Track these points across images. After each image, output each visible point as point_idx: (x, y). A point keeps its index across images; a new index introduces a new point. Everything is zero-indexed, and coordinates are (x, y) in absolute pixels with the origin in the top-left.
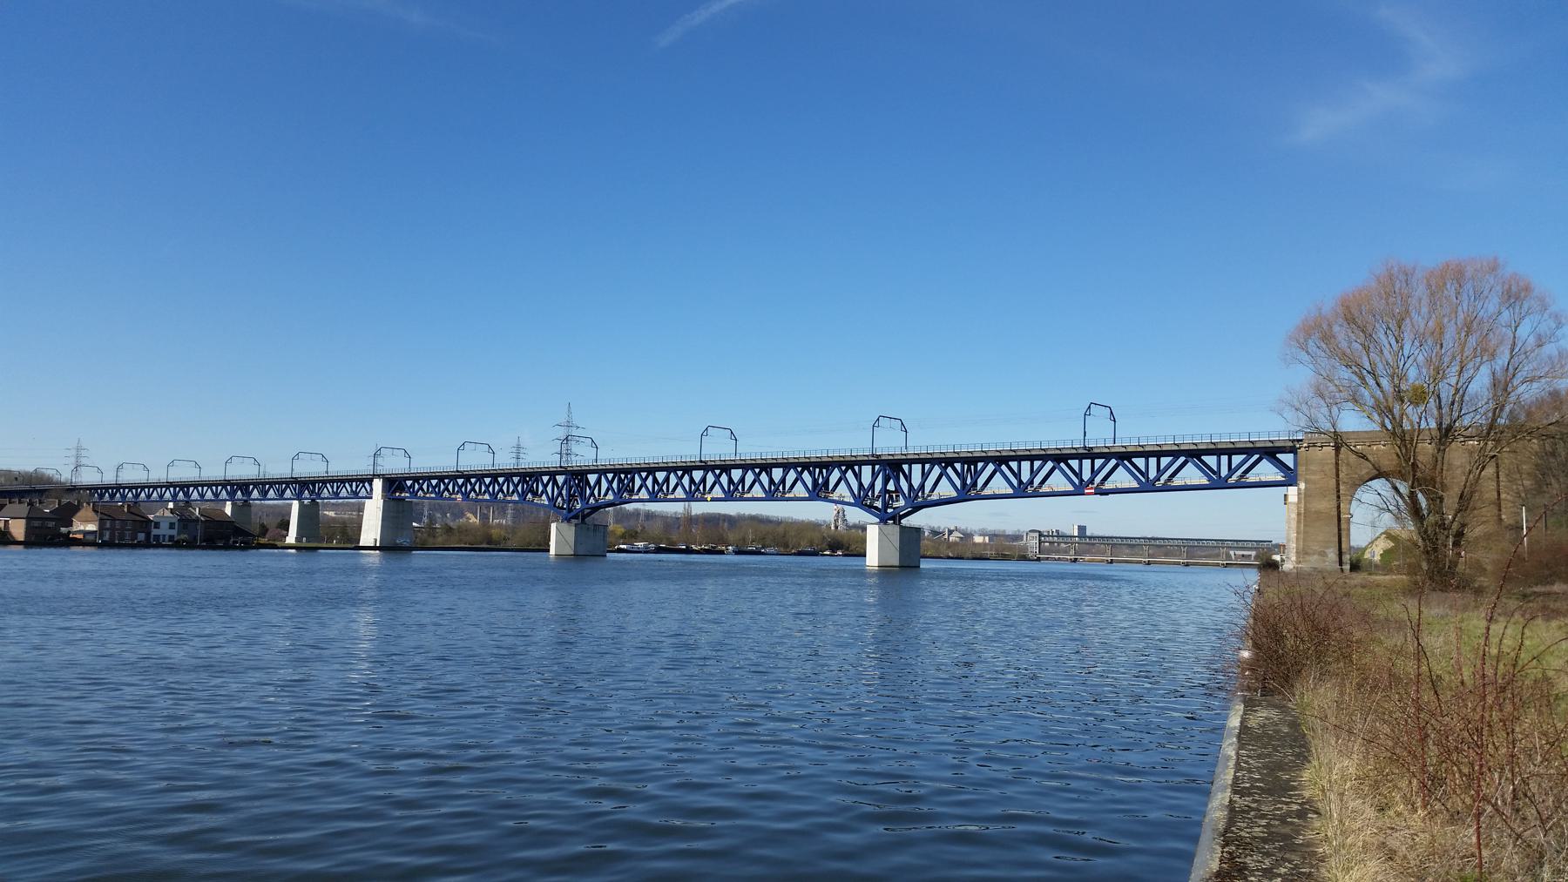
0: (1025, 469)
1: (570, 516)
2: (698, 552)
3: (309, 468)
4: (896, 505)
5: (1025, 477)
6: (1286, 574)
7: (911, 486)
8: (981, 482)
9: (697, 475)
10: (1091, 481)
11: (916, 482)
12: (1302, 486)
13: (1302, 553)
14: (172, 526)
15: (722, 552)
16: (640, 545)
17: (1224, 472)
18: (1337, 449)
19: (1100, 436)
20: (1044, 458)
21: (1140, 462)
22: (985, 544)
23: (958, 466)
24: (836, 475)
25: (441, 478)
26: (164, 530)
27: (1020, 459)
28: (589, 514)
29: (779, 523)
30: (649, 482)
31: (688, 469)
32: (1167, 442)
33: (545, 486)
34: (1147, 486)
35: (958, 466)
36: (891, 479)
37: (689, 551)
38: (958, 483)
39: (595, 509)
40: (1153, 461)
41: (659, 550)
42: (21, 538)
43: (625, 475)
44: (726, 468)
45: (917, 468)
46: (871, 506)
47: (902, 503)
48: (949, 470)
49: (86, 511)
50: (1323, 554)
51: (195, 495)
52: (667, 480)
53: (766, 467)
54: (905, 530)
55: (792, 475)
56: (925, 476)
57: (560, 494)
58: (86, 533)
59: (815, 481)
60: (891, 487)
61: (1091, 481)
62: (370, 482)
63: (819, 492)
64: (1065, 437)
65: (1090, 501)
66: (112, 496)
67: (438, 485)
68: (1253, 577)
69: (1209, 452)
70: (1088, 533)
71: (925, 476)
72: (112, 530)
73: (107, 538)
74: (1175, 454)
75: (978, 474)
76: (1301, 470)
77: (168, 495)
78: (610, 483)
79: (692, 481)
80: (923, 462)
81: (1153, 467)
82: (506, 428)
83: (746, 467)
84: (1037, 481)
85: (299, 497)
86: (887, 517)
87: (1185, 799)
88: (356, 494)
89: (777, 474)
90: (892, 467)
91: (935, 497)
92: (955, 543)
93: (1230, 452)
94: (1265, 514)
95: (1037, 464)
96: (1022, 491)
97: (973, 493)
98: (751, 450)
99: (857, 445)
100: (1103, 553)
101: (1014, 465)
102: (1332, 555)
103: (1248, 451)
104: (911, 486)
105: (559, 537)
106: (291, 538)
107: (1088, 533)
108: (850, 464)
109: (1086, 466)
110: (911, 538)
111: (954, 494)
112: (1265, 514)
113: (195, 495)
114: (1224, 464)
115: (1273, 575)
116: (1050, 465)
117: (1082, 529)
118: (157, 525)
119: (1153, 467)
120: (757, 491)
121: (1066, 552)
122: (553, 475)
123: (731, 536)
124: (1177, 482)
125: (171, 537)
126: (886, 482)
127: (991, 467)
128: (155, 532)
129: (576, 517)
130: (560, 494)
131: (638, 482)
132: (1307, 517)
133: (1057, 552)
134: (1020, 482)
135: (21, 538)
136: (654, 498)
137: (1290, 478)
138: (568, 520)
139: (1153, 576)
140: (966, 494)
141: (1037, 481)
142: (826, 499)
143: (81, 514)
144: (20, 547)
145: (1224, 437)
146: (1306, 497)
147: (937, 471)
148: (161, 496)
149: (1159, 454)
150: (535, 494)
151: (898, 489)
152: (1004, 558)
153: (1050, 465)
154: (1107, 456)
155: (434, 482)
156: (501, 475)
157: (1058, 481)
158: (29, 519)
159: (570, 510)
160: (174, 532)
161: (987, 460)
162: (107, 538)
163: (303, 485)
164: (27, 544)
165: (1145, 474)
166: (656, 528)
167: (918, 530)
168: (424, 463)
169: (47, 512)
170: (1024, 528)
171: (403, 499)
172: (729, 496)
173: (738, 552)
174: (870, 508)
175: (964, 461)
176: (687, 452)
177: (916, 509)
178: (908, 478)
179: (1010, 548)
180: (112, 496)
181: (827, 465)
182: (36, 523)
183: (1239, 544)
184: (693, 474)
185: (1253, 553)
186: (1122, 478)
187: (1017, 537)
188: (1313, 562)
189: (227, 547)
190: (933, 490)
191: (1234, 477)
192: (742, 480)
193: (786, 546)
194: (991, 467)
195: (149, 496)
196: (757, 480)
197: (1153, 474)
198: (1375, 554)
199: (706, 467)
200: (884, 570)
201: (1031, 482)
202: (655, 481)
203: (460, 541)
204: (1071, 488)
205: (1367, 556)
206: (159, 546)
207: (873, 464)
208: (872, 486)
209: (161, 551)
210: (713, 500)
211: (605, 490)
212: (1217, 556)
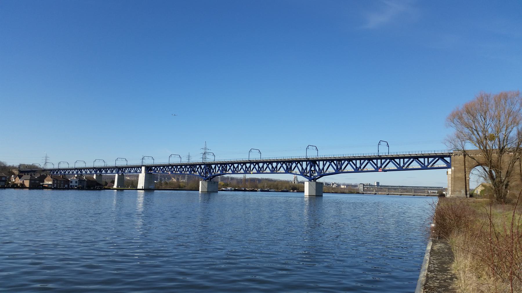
0: (359, 163)
1: (206, 179)
2: (248, 191)
4: (314, 175)
5: (358, 165)
6: (448, 198)
7: (319, 169)
9: (248, 165)
10: (381, 167)
12: (453, 168)
13: (453, 191)
14: (76, 182)
15: (256, 191)
16: (229, 188)
18: (465, 156)
19: (383, 152)
20: (365, 159)
21: (397, 160)
24: (294, 165)
25: (164, 166)
26: (74, 184)
27: (356, 159)
29: (275, 181)
30: (232, 168)
31: (245, 163)
32: (407, 154)
33: (198, 169)
34: (400, 169)
35: (335, 162)
36: (313, 166)
37: (245, 190)
38: (335, 167)
39: (214, 176)
40: (402, 160)
41: (235, 190)
42: (28, 186)
43: (224, 165)
44: (257, 163)
45: (321, 163)
46: (306, 175)
47: (316, 174)
48: (332, 163)
49: (49, 177)
50: (460, 191)
51: (84, 172)
52: (238, 167)
53: (271, 162)
54: (317, 183)
56: (324, 165)
57: (203, 171)
58: (49, 185)
59: (287, 167)
60: (313, 169)
61: (381, 167)
62: (141, 168)
63: (289, 171)
64: (372, 152)
66: (57, 173)
67: (163, 169)
68: (436, 200)
70: (380, 185)
71: (324, 165)
72: (57, 183)
73: (55, 186)
74: (409, 158)
75: (342, 164)
76: (452, 163)
77: (75, 172)
79: (246, 167)
80: (323, 160)
81: (402, 162)
83: (264, 162)
84: (362, 167)
86: (312, 179)
89: (274, 165)
90: (313, 162)
91: (327, 172)
92: (334, 188)
93: (428, 157)
94: (440, 178)
95: (362, 161)
96: (357, 170)
97: (340, 171)
98: (266, 156)
99: (301, 155)
100: (385, 191)
101: (354, 161)
102: (463, 192)
103: (434, 157)
104: (319, 169)
105: (202, 185)
107: (380, 185)
108: (299, 161)
109: (379, 162)
110: (320, 186)
111: (334, 171)
112: (440, 178)
114: (427, 161)
115: (443, 199)
116: (388, 160)
117: (378, 183)
118: (71, 182)
119: (402, 162)
121: (372, 191)
122: (200, 165)
123: (259, 185)
124: (410, 167)
126: (311, 167)
127: (346, 162)
128: (71, 184)
129: (208, 179)
130: (203, 171)
131: (228, 167)
132: (454, 179)
133: (370, 191)
134: (357, 167)
136: (233, 173)
137: (449, 166)
138: (205, 180)
140: (338, 171)
141: (362, 167)
142: (291, 173)
146: (454, 172)
147: (328, 163)
148: (73, 173)
149: (404, 158)
150: (194, 171)
151: (315, 170)
152: (351, 193)
153: (366, 161)
154: (386, 159)
159: (206, 177)
160: (77, 184)
161: (345, 160)
163: (119, 169)
164: (30, 188)
165: (399, 165)
166: (234, 183)
172: (258, 172)
174: (306, 176)
175: (337, 160)
176: (244, 157)
177: (321, 176)
178: (318, 166)
179: (353, 190)
180: (57, 173)
181: (291, 162)
182: (33, 182)
184: (246, 165)
185: (436, 191)
186: (391, 166)
187: (356, 186)
188: (457, 194)
190: (327, 170)
192: (263, 167)
193: (278, 189)
194: (346, 162)
195: (69, 172)
197: (402, 164)
198: (478, 191)
199: (251, 162)
202: (234, 167)
204: (374, 169)
207: (306, 161)
208: (306, 169)
211: (217, 170)
212: (424, 192)
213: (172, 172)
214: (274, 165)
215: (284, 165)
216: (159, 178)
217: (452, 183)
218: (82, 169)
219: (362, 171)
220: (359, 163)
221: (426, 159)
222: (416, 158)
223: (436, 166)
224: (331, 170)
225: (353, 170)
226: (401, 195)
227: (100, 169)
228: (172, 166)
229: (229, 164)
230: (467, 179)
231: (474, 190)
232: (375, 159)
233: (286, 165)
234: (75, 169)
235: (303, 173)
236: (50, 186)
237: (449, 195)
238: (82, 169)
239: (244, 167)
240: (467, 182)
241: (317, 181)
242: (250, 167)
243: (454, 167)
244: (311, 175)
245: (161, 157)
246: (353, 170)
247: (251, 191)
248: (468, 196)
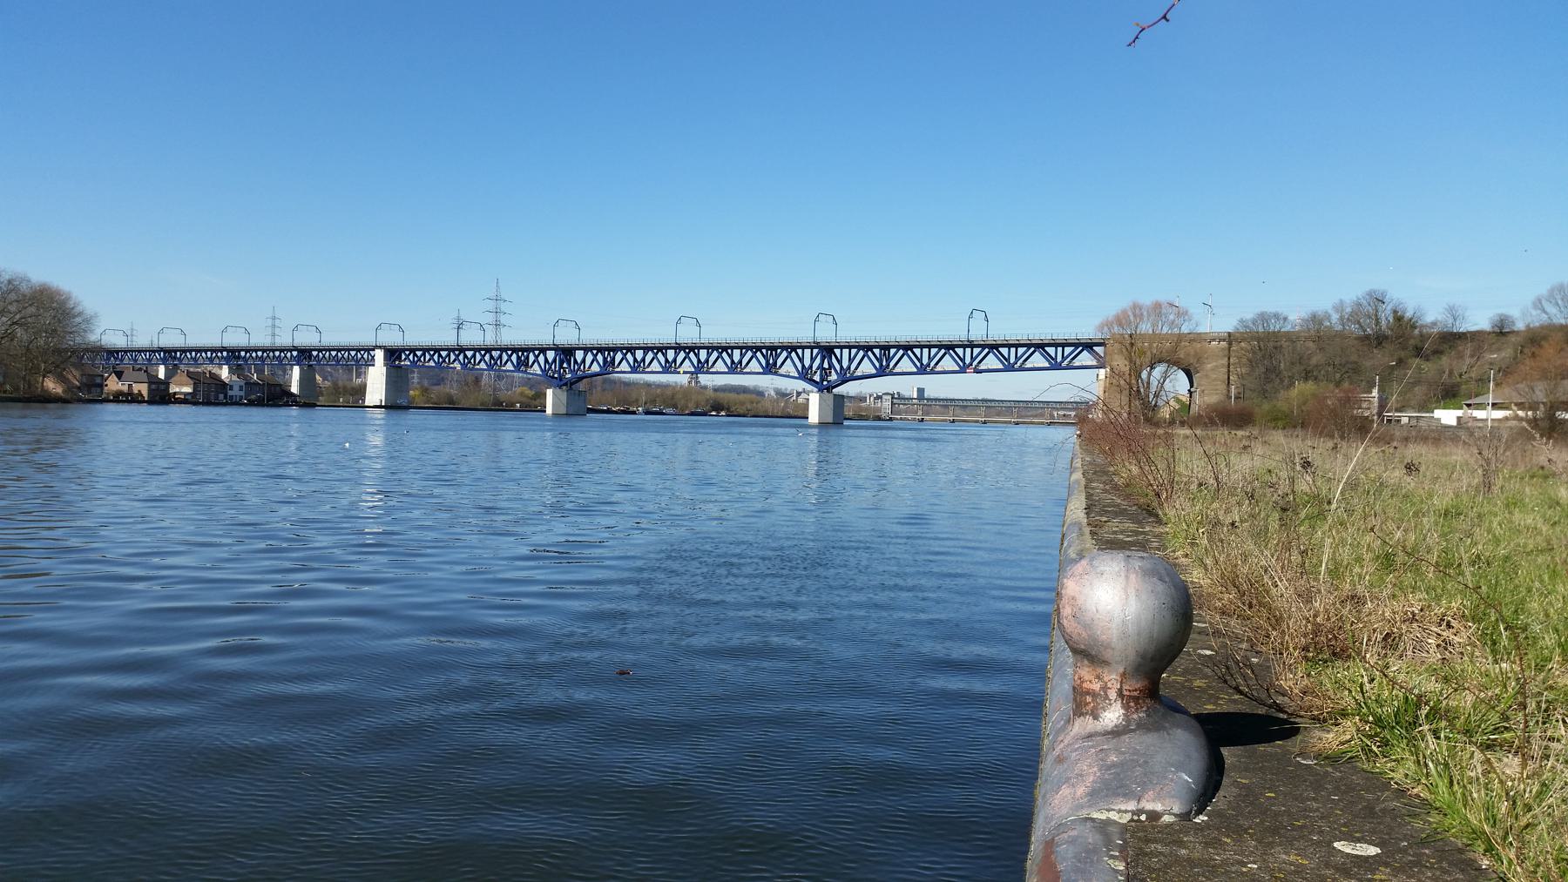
0: (926, 354)
1: (560, 383)
8: (779, 362)
9: (495, 354)
15: (634, 413)
18: (1230, 344)
19: (977, 334)
21: (1004, 351)
32: (1023, 338)
34: (1009, 368)
35: (877, 351)
36: (826, 361)
39: (581, 378)
45: (737, 353)
55: (650, 355)
56: (742, 356)
58: (186, 394)
59: (605, 359)
60: (826, 365)
63: (770, 369)
65: (970, 377)
71: (742, 356)
75: (778, 356)
80: (741, 348)
81: (1012, 354)
82: (1302, 281)
83: (710, 348)
86: (824, 388)
87: (1039, 656)
89: (639, 354)
90: (827, 350)
99: (805, 336)
124: (1028, 365)
127: (785, 354)
128: (230, 393)
131: (532, 358)
136: (634, 370)
139: (990, 434)
140: (882, 372)
141: (744, 362)
142: (776, 373)
145: (1060, 334)
147: (749, 354)
151: (831, 365)
154: (983, 347)
158: (150, 383)
161: (784, 348)
168: (412, 339)
173: (648, 413)
174: (811, 381)
176: (665, 336)
181: (615, 349)
186: (992, 361)
199: (678, 348)
200: (822, 425)
207: (812, 348)
212: (1042, 415)
214: (639, 354)
215: (629, 356)
216: (434, 382)
219: (933, 372)
222: (1040, 346)
223: (1077, 363)
224: (867, 367)
232: (1003, 346)
235: (805, 375)
239: (487, 357)
244: (822, 379)
245: (427, 328)
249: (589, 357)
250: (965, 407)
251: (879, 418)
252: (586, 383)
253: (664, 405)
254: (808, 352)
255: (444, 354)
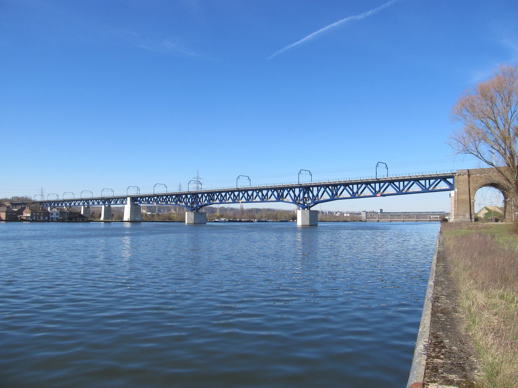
0: (354, 188)
1: (192, 209)
2: (244, 222)
3: (108, 194)
4: (308, 202)
5: (355, 190)
6: (451, 223)
7: (313, 195)
10: (379, 191)
11: (297, 194)
12: (456, 190)
13: (456, 215)
14: (57, 214)
15: (253, 222)
16: (223, 219)
17: (427, 186)
18: (469, 176)
19: (382, 175)
20: (362, 183)
21: (397, 184)
22: (347, 216)
23: (330, 187)
24: (286, 192)
25: (149, 197)
26: (54, 216)
27: (353, 184)
28: (199, 209)
29: (274, 210)
30: (232, 196)
31: (233, 192)
32: (406, 175)
33: (184, 199)
34: (400, 193)
35: (330, 187)
37: (240, 221)
38: (330, 193)
39: (201, 207)
40: (401, 183)
41: (229, 221)
42: (4, 219)
43: (211, 194)
44: (246, 191)
45: (315, 189)
46: (299, 203)
47: (310, 202)
48: (327, 189)
49: (27, 209)
50: (464, 215)
51: (91, 203)
52: (239, 195)
53: (261, 190)
54: (311, 212)
55: (270, 193)
56: (318, 191)
57: (189, 201)
59: (278, 194)
61: (379, 191)
62: (126, 198)
63: (280, 198)
64: (370, 176)
65: (379, 199)
66: (62, 204)
67: (157, 199)
68: (438, 226)
69: (422, 179)
70: (383, 211)
71: (318, 191)
72: (36, 216)
73: (34, 218)
74: (409, 180)
75: (338, 190)
76: (456, 184)
77: (81, 204)
78: (206, 197)
79: (248, 195)
81: (401, 185)
83: (253, 190)
84: (360, 192)
85: (104, 204)
88: (122, 203)
89: (265, 192)
90: (307, 189)
91: (322, 199)
92: (337, 216)
93: (429, 179)
94: (442, 202)
95: (359, 185)
96: (354, 196)
97: (336, 197)
98: (255, 184)
99: (293, 181)
100: (388, 218)
101: (351, 186)
102: (468, 215)
103: (436, 178)
104: (313, 195)
105: (189, 217)
106: (102, 218)
107: (383, 211)
108: (292, 188)
109: (377, 186)
110: (314, 215)
111: (329, 198)
112: (442, 202)
113: (91, 203)
114: (427, 183)
115: (446, 224)
116: (387, 184)
117: (381, 210)
118: (52, 214)
119: (401, 185)
120: (258, 199)
121: (376, 218)
122: (186, 195)
123: (257, 216)
124: (411, 190)
125: (57, 218)
126: (304, 194)
127: (342, 188)
128: (51, 216)
129: (194, 210)
130: (189, 201)
131: (216, 197)
132: (458, 202)
133: (373, 218)
134: (353, 192)
135: (4, 219)
137: (452, 187)
138: (192, 211)
140: (333, 198)
141: (360, 192)
142: (282, 201)
143: (26, 210)
144: (4, 222)
145: (427, 172)
146: (458, 194)
147: (323, 189)
148: (79, 204)
149: (404, 181)
150: (181, 202)
152: (354, 221)
153: (364, 186)
154: (385, 182)
155: (156, 198)
156: (174, 195)
157: (367, 192)
158: (7, 212)
159: (192, 207)
160: (58, 216)
161: (341, 185)
162: (34, 218)
163: (106, 200)
164: (6, 221)
165: (399, 188)
166: (231, 214)
167: (317, 212)
168: (144, 192)
169: (15, 211)
170: (361, 211)
171: (137, 204)
172: (262, 200)
173: (258, 221)
175: (333, 185)
177: (316, 204)
178: (312, 192)
179: (356, 218)
180: (62, 204)
181: (283, 188)
182: (9, 214)
183: (434, 213)
184: (235, 194)
185: (439, 216)
186: (391, 190)
187: (360, 214)
188: (461, 218)
189: (76, 221)
190: (321, 197)
191: (431, 188)
192: (267, 194)
193: (277, 219)
194: (342, 188)
195: (75, 204)
196: (258, 195)
197: (401, 188)
198: (481, 215)
199: (239, 191)
200: (304, 227)
201: (357, 192)
202: (234, 195)
203: (160, 219)
204: (372, 194)
205: (478, 216)
206: (52, 221)
207: (299, 187)
208: (299, 195)
209: (53, 223)
210: (242, 202)
211: (204, 200)
213: (167, 203)
217: (455, 206)
218: (88, 200)
220: (354, 188)
221: (427, 181)
222: (417, 180)
224: (326, 196)
225: (350, 196)
226: (416, 221)
227: (87, 200)
228: (158, 196)
229: (216, 192)
230: (472, 201)
231: (477, 214)
232: (396, 181)
233: (277, 192)
234: (81, 200)
235: (295, 201)
236: (28, 219)
237: (452, 219)
238: (88, 200)
239: (246, 195)
240: (472, 205)
241: (312, 209)
242: (252, 194)
243: (458, 189)
244: (304, 203)
246: (350, 196)
247: (247, 221)
248: (473, 220)
249: (270, 193)
250: (398, 215)
251: (361, 221)
252: (71, 214)
253: (235, 218)
254: (377, 185)
255: (223, 194)
